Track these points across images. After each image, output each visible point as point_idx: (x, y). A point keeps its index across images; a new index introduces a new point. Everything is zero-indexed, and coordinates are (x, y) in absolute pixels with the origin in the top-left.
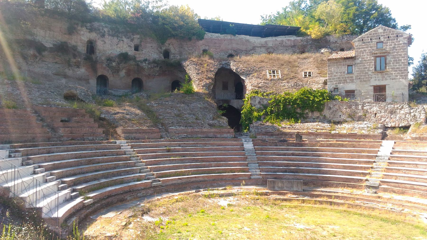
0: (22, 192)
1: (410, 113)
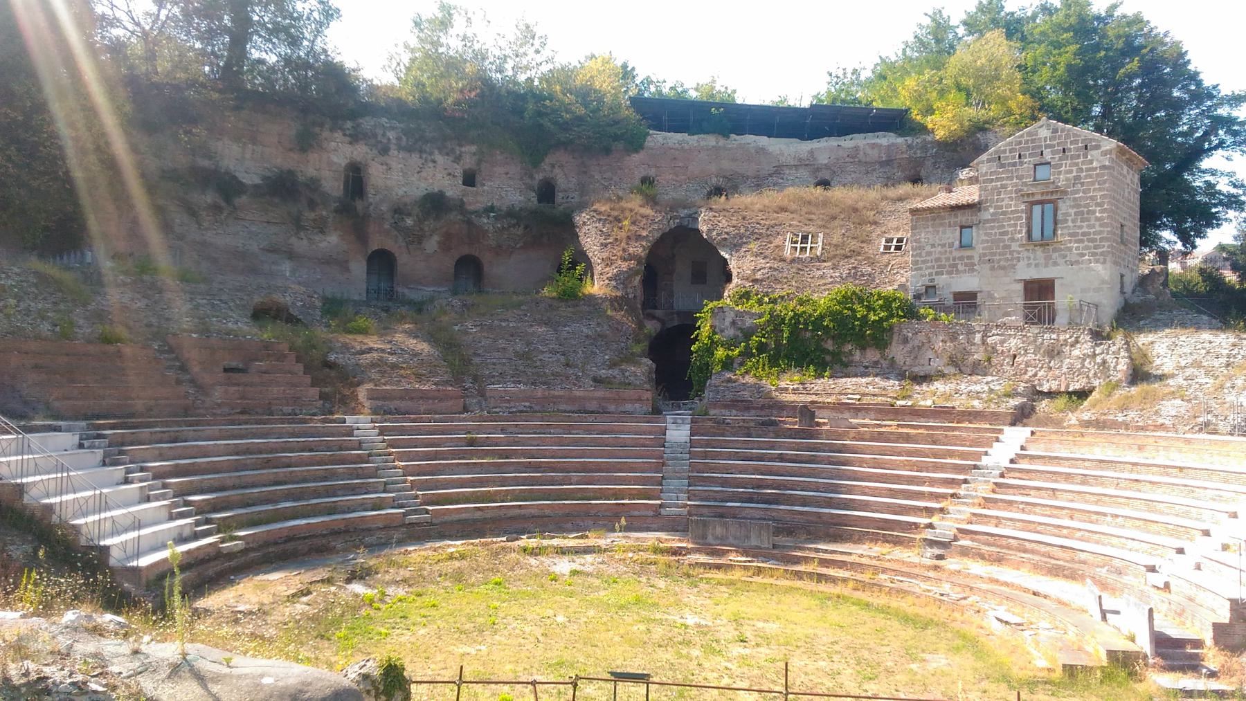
0: (75, 517)
1: (1094, 355)
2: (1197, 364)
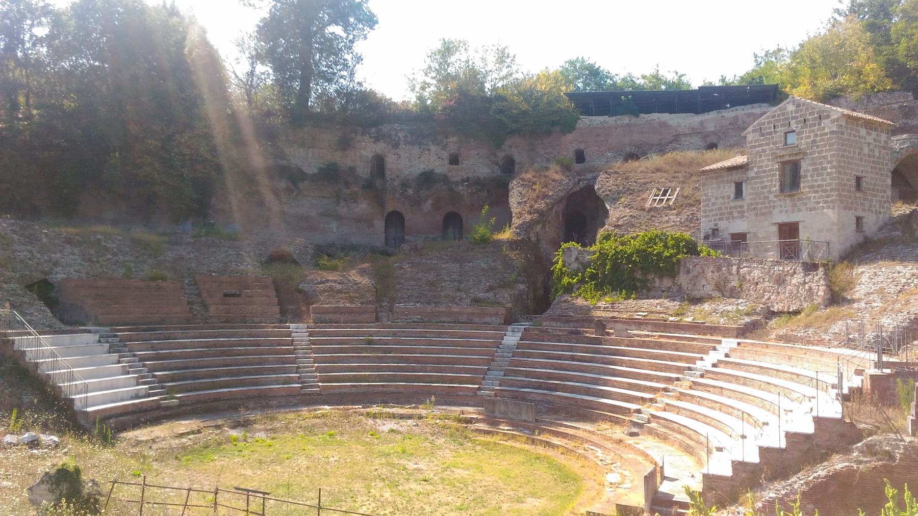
1: (805, 283)
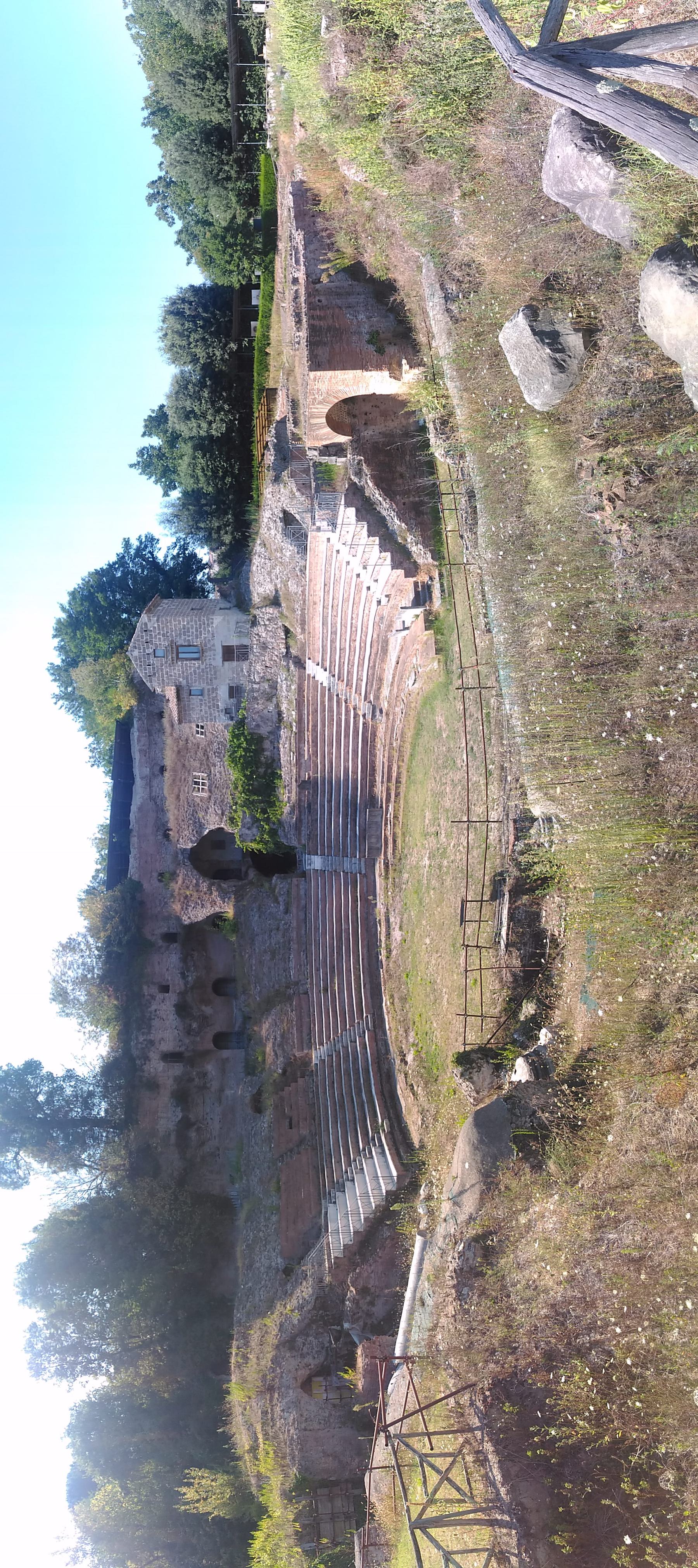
1: (265, 625)
2: (269, 573)
